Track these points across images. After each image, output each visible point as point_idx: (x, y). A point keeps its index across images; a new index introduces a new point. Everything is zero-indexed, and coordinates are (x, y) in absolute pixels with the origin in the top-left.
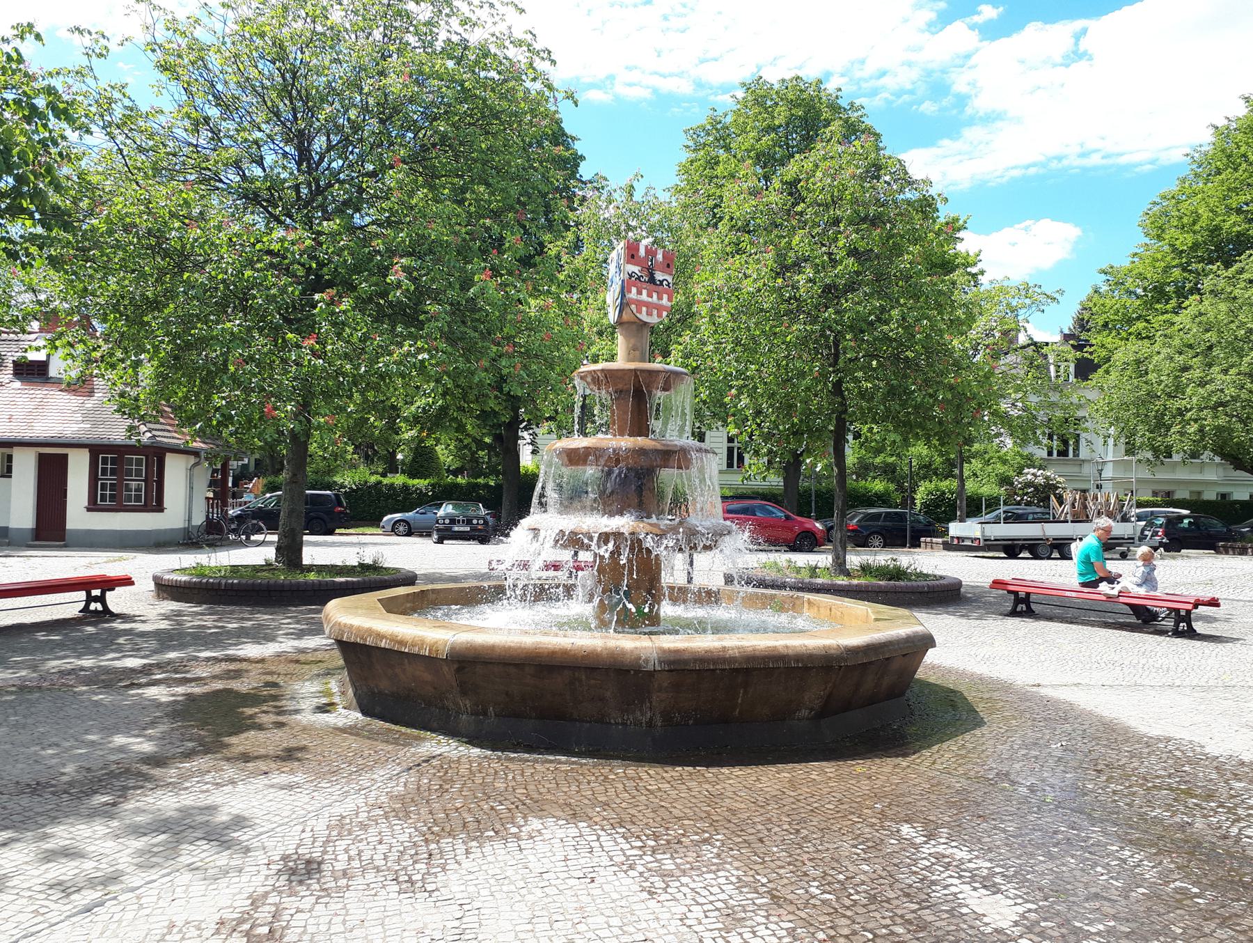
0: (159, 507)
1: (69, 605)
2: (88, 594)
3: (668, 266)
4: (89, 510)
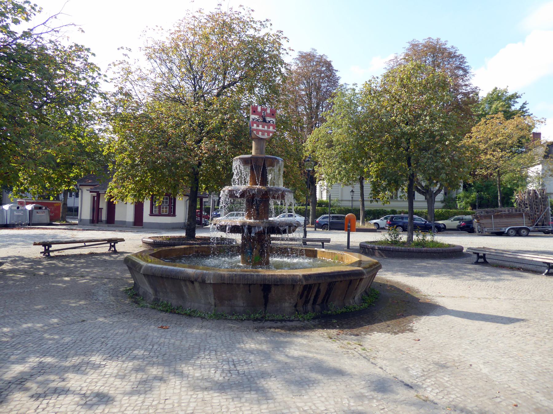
0: (174, 215)
1: (105, 249)
3: (273, 115)
4: (150, 215)
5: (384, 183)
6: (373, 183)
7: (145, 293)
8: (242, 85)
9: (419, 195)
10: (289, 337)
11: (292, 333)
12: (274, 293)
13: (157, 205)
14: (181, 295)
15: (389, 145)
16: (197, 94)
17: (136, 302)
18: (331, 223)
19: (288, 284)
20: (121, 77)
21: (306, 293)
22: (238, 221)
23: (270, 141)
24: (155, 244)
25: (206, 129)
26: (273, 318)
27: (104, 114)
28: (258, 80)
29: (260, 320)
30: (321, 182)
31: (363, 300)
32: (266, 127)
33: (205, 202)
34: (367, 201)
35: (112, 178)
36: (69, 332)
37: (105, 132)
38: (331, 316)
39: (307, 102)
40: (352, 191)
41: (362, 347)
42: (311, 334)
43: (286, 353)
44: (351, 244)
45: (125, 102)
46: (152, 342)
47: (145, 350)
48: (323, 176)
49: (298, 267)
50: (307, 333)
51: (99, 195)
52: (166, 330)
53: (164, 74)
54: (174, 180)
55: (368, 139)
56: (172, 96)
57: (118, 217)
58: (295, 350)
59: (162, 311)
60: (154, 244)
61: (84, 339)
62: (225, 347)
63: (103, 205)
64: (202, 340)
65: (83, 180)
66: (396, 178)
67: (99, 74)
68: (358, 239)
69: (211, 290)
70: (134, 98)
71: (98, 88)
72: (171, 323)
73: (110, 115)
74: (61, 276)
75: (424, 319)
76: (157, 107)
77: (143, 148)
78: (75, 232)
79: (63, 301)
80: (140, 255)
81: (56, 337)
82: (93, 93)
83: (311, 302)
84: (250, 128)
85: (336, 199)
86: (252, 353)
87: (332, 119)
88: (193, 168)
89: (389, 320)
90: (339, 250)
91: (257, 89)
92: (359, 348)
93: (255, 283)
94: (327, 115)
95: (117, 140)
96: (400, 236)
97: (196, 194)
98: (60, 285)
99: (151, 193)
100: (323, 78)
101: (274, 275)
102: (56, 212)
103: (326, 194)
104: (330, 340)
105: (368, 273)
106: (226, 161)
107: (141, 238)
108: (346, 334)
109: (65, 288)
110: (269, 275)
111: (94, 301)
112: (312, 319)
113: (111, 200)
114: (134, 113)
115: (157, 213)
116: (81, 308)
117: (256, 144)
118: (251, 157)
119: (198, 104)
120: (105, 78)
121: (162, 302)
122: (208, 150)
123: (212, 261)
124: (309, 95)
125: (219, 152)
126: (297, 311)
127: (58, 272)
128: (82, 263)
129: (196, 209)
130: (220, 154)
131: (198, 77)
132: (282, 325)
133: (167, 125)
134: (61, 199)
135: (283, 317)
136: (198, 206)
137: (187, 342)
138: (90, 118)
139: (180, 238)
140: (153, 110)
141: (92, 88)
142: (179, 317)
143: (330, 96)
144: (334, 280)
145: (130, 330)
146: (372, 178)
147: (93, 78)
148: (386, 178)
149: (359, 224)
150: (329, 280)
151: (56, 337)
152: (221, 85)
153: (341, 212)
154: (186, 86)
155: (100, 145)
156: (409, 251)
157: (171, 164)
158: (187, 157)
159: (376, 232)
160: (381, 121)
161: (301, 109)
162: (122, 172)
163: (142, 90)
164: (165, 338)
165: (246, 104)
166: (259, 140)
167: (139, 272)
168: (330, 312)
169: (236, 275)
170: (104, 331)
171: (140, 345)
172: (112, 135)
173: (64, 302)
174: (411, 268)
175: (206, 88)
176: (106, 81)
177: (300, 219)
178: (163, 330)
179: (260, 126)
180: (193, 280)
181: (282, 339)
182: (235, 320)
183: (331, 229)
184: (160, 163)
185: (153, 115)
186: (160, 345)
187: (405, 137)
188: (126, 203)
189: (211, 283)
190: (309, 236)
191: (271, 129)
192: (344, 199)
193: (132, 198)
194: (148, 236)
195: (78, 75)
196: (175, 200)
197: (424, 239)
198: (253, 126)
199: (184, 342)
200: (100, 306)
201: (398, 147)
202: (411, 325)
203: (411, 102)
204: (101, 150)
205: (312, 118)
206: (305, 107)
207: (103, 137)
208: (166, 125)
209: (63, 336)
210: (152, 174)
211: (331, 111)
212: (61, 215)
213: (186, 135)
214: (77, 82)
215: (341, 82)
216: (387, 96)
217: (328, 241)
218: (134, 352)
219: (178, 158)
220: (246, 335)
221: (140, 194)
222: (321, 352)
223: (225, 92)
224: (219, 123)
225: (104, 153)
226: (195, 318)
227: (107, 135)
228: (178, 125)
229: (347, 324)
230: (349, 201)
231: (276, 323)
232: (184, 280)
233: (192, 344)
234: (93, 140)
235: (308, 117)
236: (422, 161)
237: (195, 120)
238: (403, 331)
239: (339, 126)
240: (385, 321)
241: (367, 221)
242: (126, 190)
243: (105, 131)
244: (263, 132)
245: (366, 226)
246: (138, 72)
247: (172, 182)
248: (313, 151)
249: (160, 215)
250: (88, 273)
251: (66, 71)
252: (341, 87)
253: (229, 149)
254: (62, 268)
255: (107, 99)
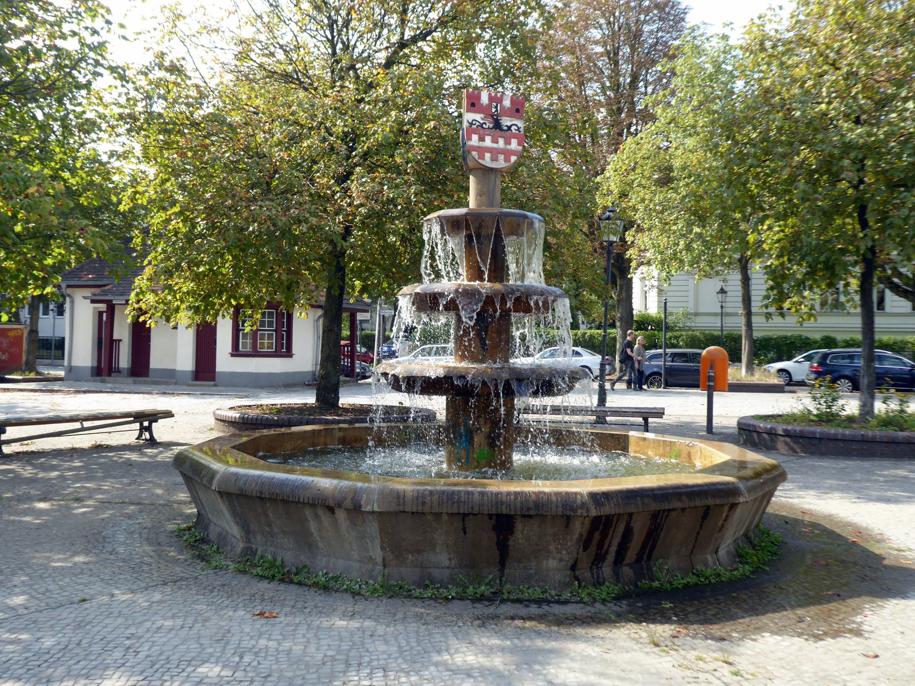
0: (289, 354)
1: (128, 435)
2: (141, 424)
3: (518, 111)
4: (233, 355)
5: (799, 270)
6: (771, 272)
7: (223, 538)
8: (445, 38)
9: (896, 298)
10: (556, 639)
11: (563, 630)
12: (522, 534)
13: (248, 329)
14: (305, 542)
15: (811, 176)
16: (337, 62)
17: (203, 558)
18: (670, 371)
19: (557, 514)
20: (160, 28)
21: (597, 536)
22: (435, 365)
23: (513, 172)
24: (244, 424)
25: (361, 149)
26: (520, 596)
27: (121, 117)
28: (483, 23)
29: (488, 599)
30: (643, 269)
31: (739, 556)
32: (501, 142)
33: (361, 321)
34: (758, 314)
35: (143, 268)
36: (52, 626)
37: (126, 162)
38: (658, 594)
39: (607, 72)
40: (722, 291)
41: (732, 669)
42: (610, 635)
43: (549, 677)
44: (716, 421)
45: (170, 86)
46: (239, 647)
47: (224, 667)
48: (648, 255)
49: (585, 476)
50: (601, 632)
51: (111, 309)
52: (272, 621)
53: (260, 17)
54: (289, 272)
55: (755, 162)
56: (279, 69)
57: (157, 361)
58: (572, 670)
59: (262, 577)
60: (243, 423)
61: (84, 641)
62: (405, 661)
63: (122, 332)
64: (354, 643)
65: (75, 273)
66: (828, 259)
67: (108, 22)
68: (732, 408)
69: (373, 527)
70: (190, 78)
71: (107, 56)
72: (283, 606)
73: (136, 119)
74: (30, 499)
75: (894, 606)
76: (244, 97)
77: (213, 197)
78: (57, 398)
79: (37, 555)
80: (210, 447)
81: (24, 637)
82: (95, 67)
83: (611, 557)
84: (464, 144)
85: (681, 311)
86: (469, 676)
87: (670, 113)
88: (332, 242)
89: (801, 606)
90: (684, 437)
91: (482, 46)
92: (726, 670)
93: (476, 510)
94: (657, 103)
95: (152, 177)
96: (841, 402)
97: (341, 303)
98: (28, 519)
99: (234, 303)
100: (648, 10)
101: (522, 493)
102: (14, 350)
103: (656, 299)
104: (656, 649)
105: (750, 490)
106: (409, 223)
107: (213, 408)
108: (694, 637)
109: (38, 527)
110: (509, 494)
111: (108, 556)
112: (615, 599)
113: (141, 319)
114: (192, 114)
115: (249, 349)
116: (76, 571)
117: (479, 182)
118: (466, 214)
119: (342, 87)
120: (122, 32)
121: (262, 557)
122: (367, 198)
123: (377, 460)
124: (613, 56)
125: (391, 201)
126: (577, 578)
127: (22, 490)
128: (75, 468)
129: (339, 337)
130: (396, 206)
131: (340, 23)
132: (540, 611)
133: (270, 138)
134: (23, 320)
135: (543, 592)
136: (346, 333)
137: (317, 649)
138: (88, 127)
139: (303, 409)
140: (236, 104)
141: (92, 55)
142: (300, 590)
143: (665, 55)
144: (666, 506)
145: (190, 621)
146: (770, 256)
147: (95, 32)
148: (803, 259)
149: (738, 373)
150: (654, 506)
151: (24, 637)
152: (394, 39)
153: (695, 342)
154: (311, 42)
155: (115, 188)
156: (864, 440)
157: (279, 235)
158: (317, 216)
159: (784, 392)
160: (788, 117)
161: (592, 89)
162: (164, 251)
163: (209, 57)
164: (269, 639)
165: (457, 83)
166: (487, 171)
167: (208, 488)
168: (656, 584)
169: (431, 492)
170: (130, 622)
171: (211, 655)
172: (143, 167)
173: (39, 558)
174: (869, 481)
175: (360, 47)
176: (124, 38)
177: (592, 360)
178: (263, 621)
179: (488, 139)
180: (332, 504)
181: (539, 643)
182: (431, 598)
183: (667, 385)
184: (253, 232)
185: (236, 118)
186: (256, 654)
187: (852, 155)
188: (175, 328)
189: (373, 512)
190: (614, 401)
191: (514, 145)
192: (701, 310)
193: (190, 313)
194: (227, 405)
195: (60, 26)
196: (290, 317)
197: (902, 411)
198: (470, 139)
199: (312, 648)
200: (119, 567)
201: (835, 179)
202: (858, 619)
203: (867, 65)
204: (114, 199)
205: (620, 111)
206: (603, 88)
207: (119, 171)
208: (267, 140)
209: (40, 634)
210: (234, 257)
211: (667, 92)
212: (24, 358)
213: (315, 162)
214: (59, 43)
215: (691, 20)
216: (805, 53)
217: (660, 413)
218: (200, 670)
219: (295, 229)
220: (455, 634)
221: (209, 305)
222: (632, 676)
223: (405, 55)
224: (391, 131)
225: (121, 208)
226: (338, 594)
227: (129, 167)
228: (294, 139)
229: (697, 612)
230: (715, 314)
231: (527, 606)
232: (313, 505)
233: (330, 653)
234: (97, 179)
235: (611, 112)
236: (896, 216)
237: (335, 125)
238: (836, 634)
239: (690, 131)
240: (793, 608)
241: (760, 364)
242: (175, 297)
243: (125, 156)
244: (495, 153)
245: (757, 378)
246: (198, 16)
247: (284, 277)
248: (623, 195)
249: (255, 354)
250: (91, 493)
251: (33, 18)
252: (693, 30)
253: (416, 194)
254: (32, 481)
255: (127, 82)
